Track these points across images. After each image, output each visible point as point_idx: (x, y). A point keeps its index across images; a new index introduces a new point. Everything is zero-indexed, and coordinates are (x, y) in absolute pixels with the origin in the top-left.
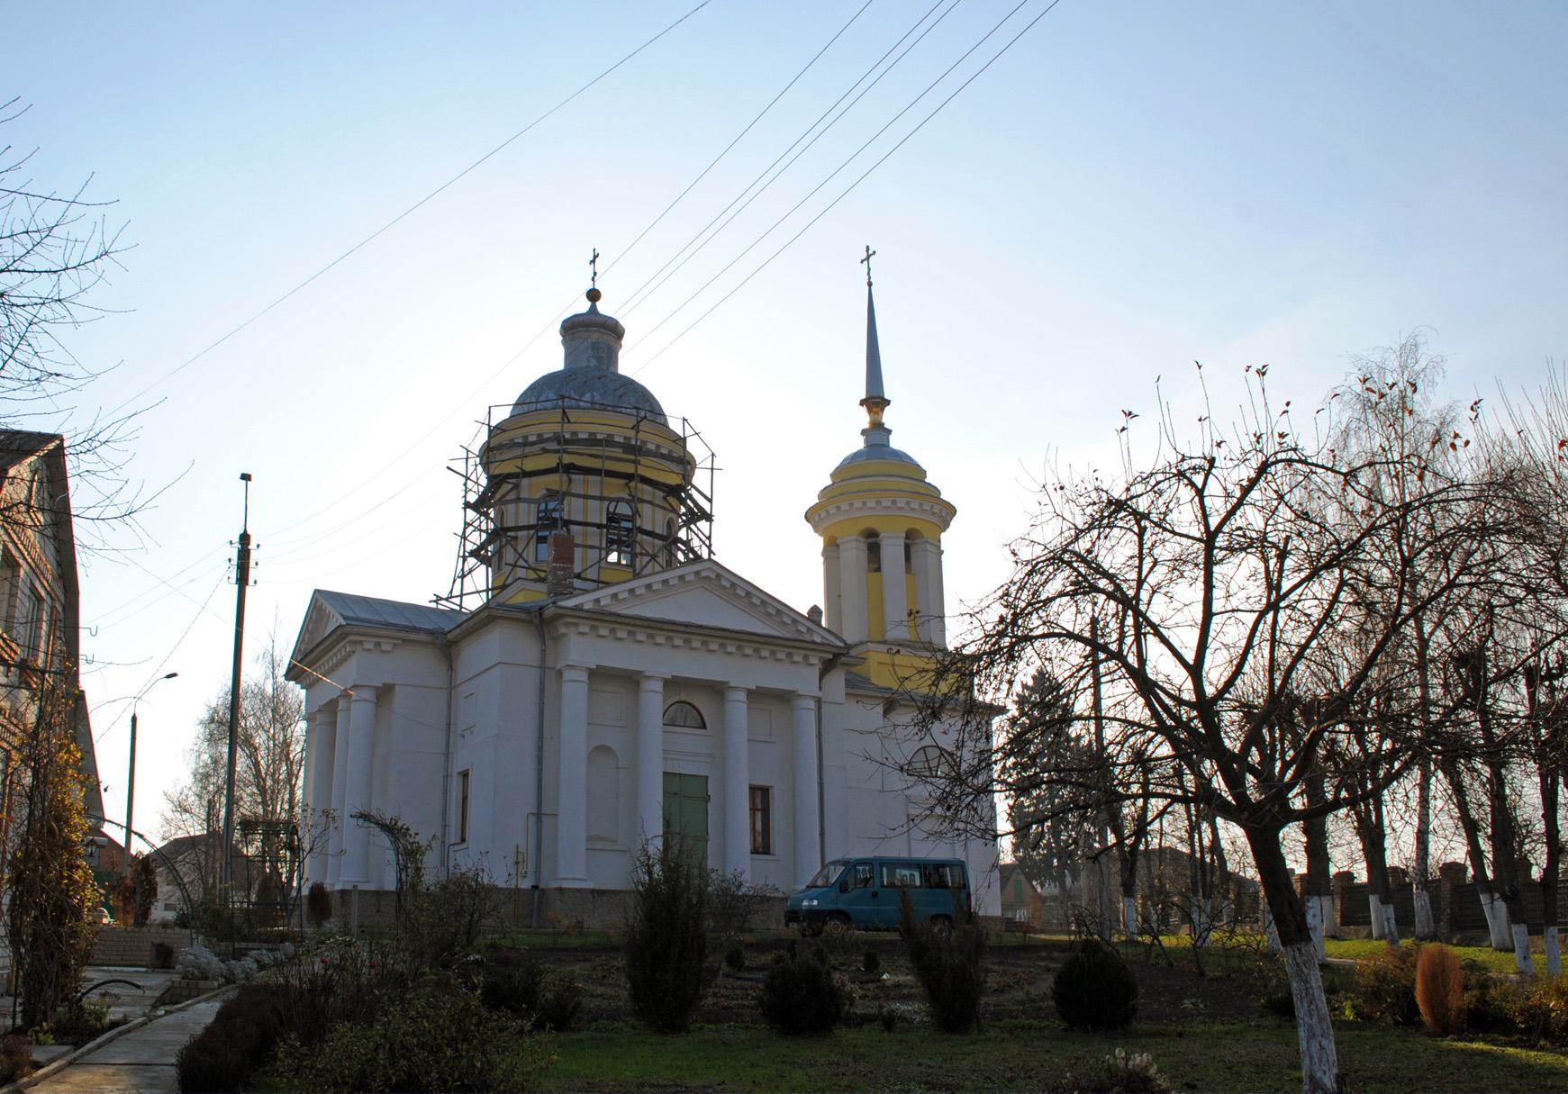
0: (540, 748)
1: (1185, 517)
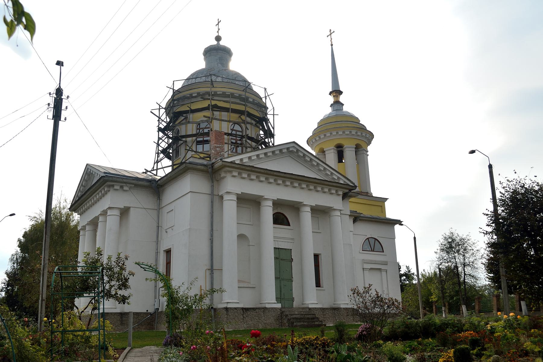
0: (212, 235)
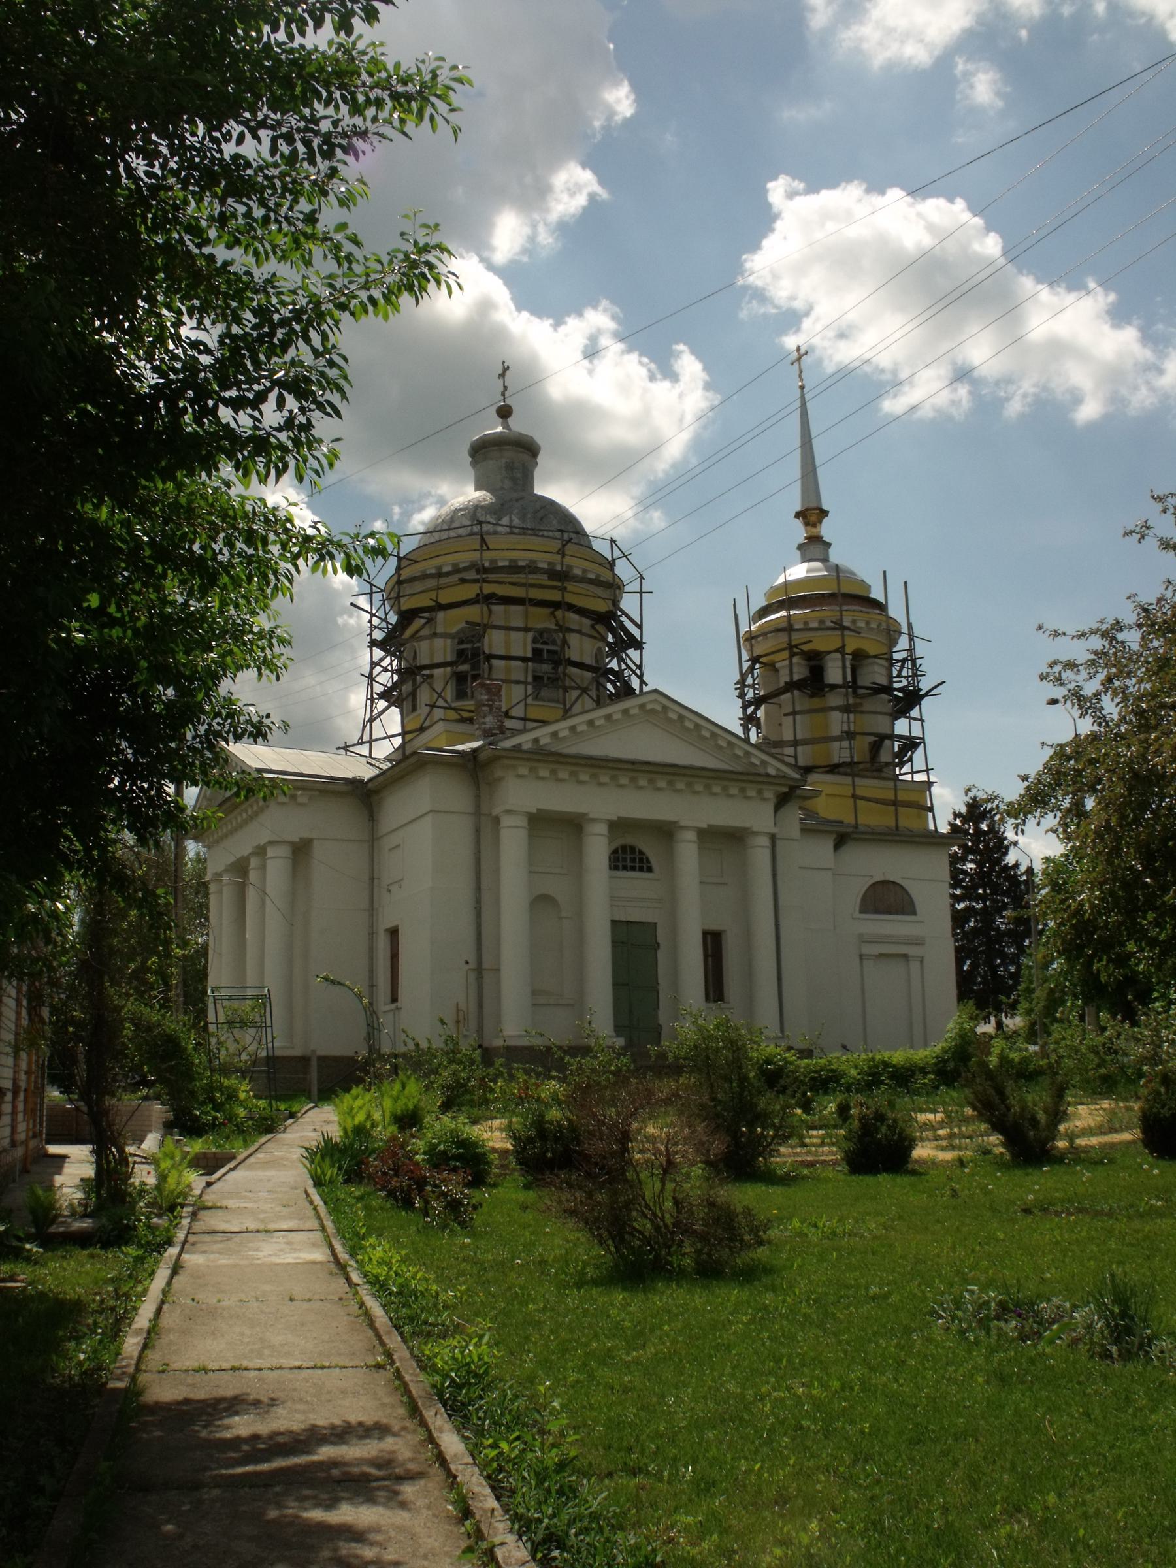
0: (478, 901)
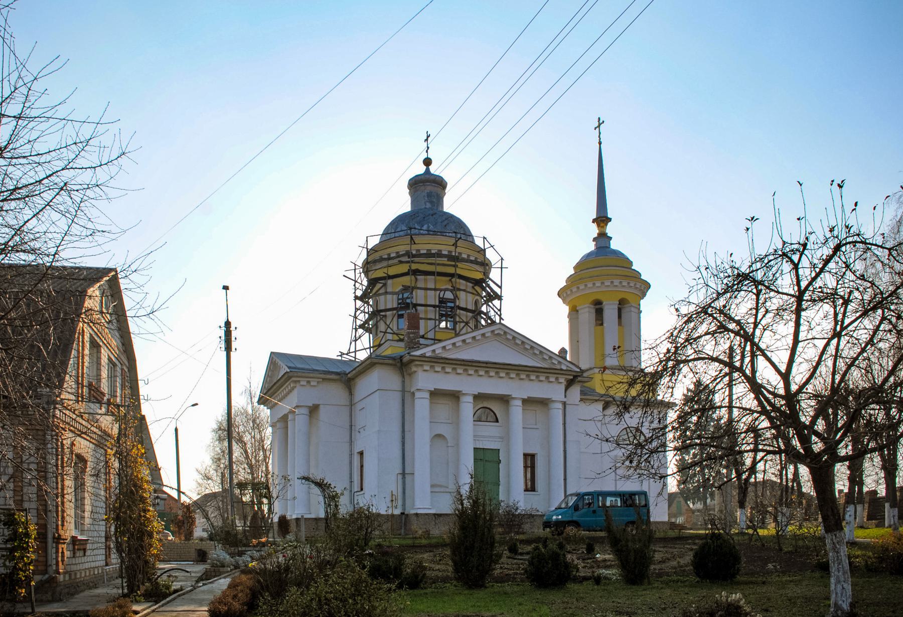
0: (403, 438)
1: (786, 283)
